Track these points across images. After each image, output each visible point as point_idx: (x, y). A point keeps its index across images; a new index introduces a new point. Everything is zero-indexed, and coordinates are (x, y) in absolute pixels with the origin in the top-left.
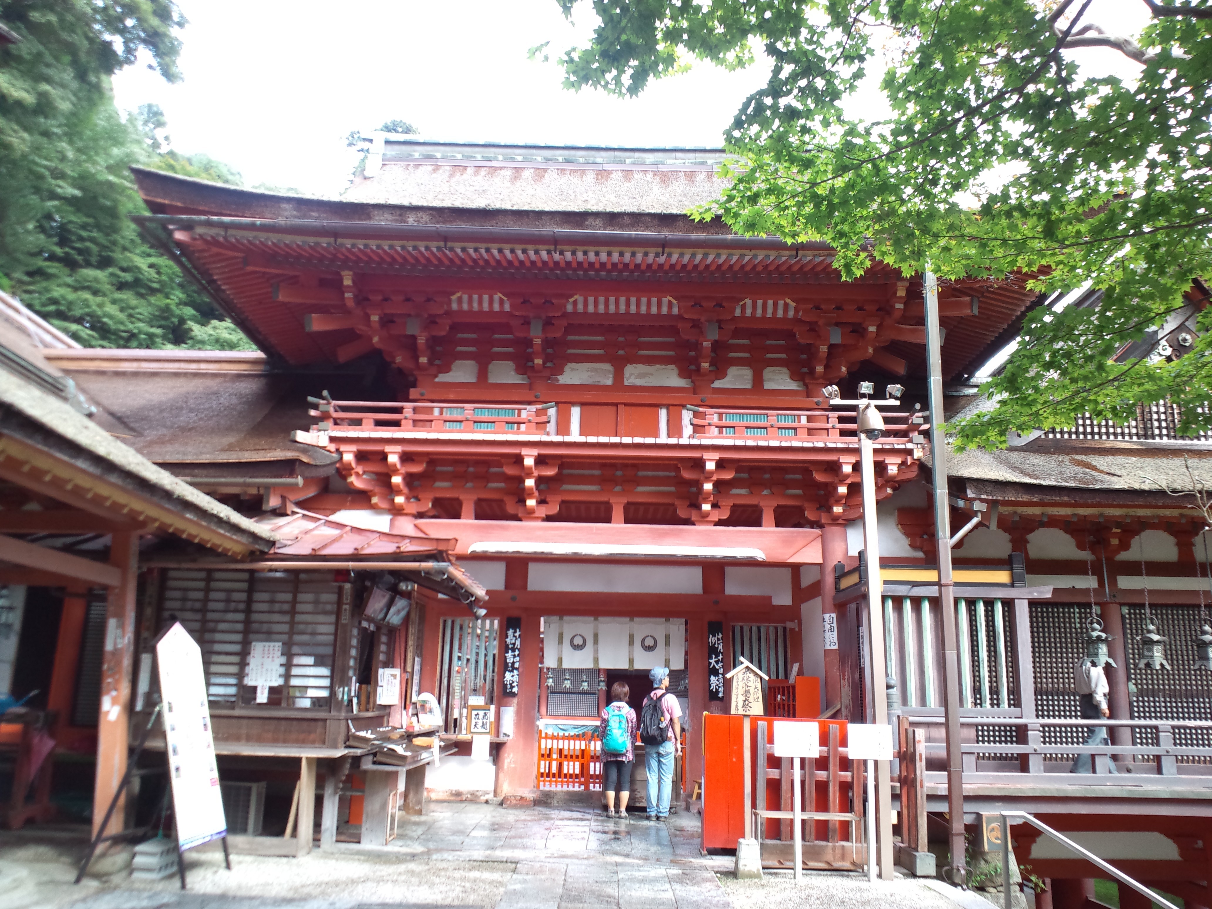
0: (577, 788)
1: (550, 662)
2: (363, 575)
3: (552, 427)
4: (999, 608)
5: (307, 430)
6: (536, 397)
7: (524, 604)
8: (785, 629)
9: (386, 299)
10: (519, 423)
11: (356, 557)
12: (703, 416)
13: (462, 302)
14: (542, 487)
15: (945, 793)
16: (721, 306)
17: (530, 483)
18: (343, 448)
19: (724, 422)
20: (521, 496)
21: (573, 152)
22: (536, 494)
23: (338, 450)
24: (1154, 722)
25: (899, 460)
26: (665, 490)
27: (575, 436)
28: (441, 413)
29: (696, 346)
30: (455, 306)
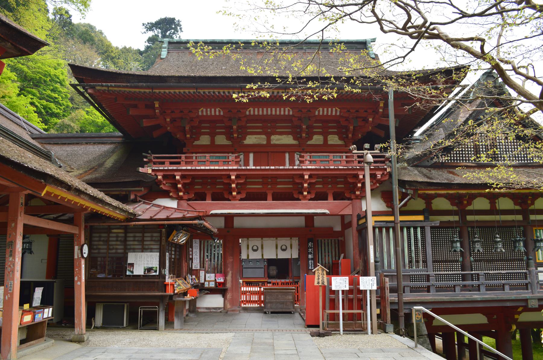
0: (256, 305)
1: (244, 256)
2: (170, 226)
3: (242, 163)
4: (419, 229)
7: (232, 234)
8: (338, 240)
9: (172, 112)
10: (228, 162)
11: (168, 219)
12: (303, 157)
13: (203, 112)
14: (239, 187)
16: (310, 111)
17: (234, 186)
18: (158, 174)
19: (312, 159)
20: (230, 191)
22: (236, 190)
23: (155, 175)
24: (478, 272)
25: (381, 173)
26: (289, 189)
28: (196, 158)
29: (300, 127)
30: (200, 114)
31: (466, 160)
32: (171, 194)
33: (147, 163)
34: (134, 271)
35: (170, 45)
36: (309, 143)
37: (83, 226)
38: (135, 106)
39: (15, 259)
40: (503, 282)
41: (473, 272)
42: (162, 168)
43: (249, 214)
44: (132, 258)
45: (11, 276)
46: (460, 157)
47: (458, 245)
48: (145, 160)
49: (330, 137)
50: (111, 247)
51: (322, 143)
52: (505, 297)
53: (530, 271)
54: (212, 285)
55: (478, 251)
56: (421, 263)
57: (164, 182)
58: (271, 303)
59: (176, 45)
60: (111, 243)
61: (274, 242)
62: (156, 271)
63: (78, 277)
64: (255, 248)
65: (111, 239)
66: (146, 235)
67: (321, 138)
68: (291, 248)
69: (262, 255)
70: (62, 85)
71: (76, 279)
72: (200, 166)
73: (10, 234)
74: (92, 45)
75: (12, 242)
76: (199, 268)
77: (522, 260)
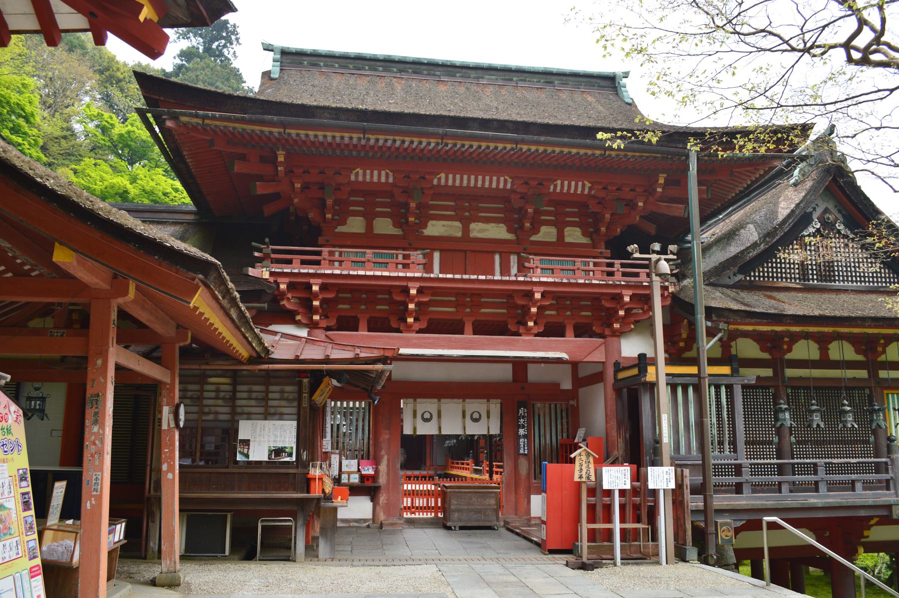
4: (723, 389)
5: (253, 267)
6: (409, 244)
13: (359, 175)
15: (702, 508)
16: (424, 178)
18: (279, 280)
21: (418, 67)
23: (275, 282)
24: (814, 461)
26: (506, 315)
27: (436, 273)
29: (406, 205)
31: (786, 278)
32: (298, 318)
33: (260, 260)
34: (251, 453)
35: (284, 57)
36: (534, 238)
37: (177, 371)
38: (243, 157)
39: (104, 430)
40: (853, 477)
41: (796, 461)
42: (288, 271)
43: (434, 356)
44: (245, 430)
45: (97, 463)
46: (777, 272)
47: (787, 415)
48: (256, 254)
49: (568, 230)
50: (206, 410)
51: (554, 240)
52: (858, 501)
53: (892, 460)
54: (355, 479)
55: (818, 425)
56: (727, 446)
57: (289, 296)
58: (459, 511)
59: (295, 57)
60: (206, 402)
61: (460, 406)
62: (290, 455)
63: (169, 464)
64: (427, 416)
65: (206, 394)
66: (272, 388)
67: (553, 230)
68: (488, 417)
69: (440, 428)
70: (27, 121)
71: (165, 467)
72: (357, 270)
73: (93, 380)
74: (84, 55)
75: (98, 395)
76: (329, 449)
77: (867, 442)
